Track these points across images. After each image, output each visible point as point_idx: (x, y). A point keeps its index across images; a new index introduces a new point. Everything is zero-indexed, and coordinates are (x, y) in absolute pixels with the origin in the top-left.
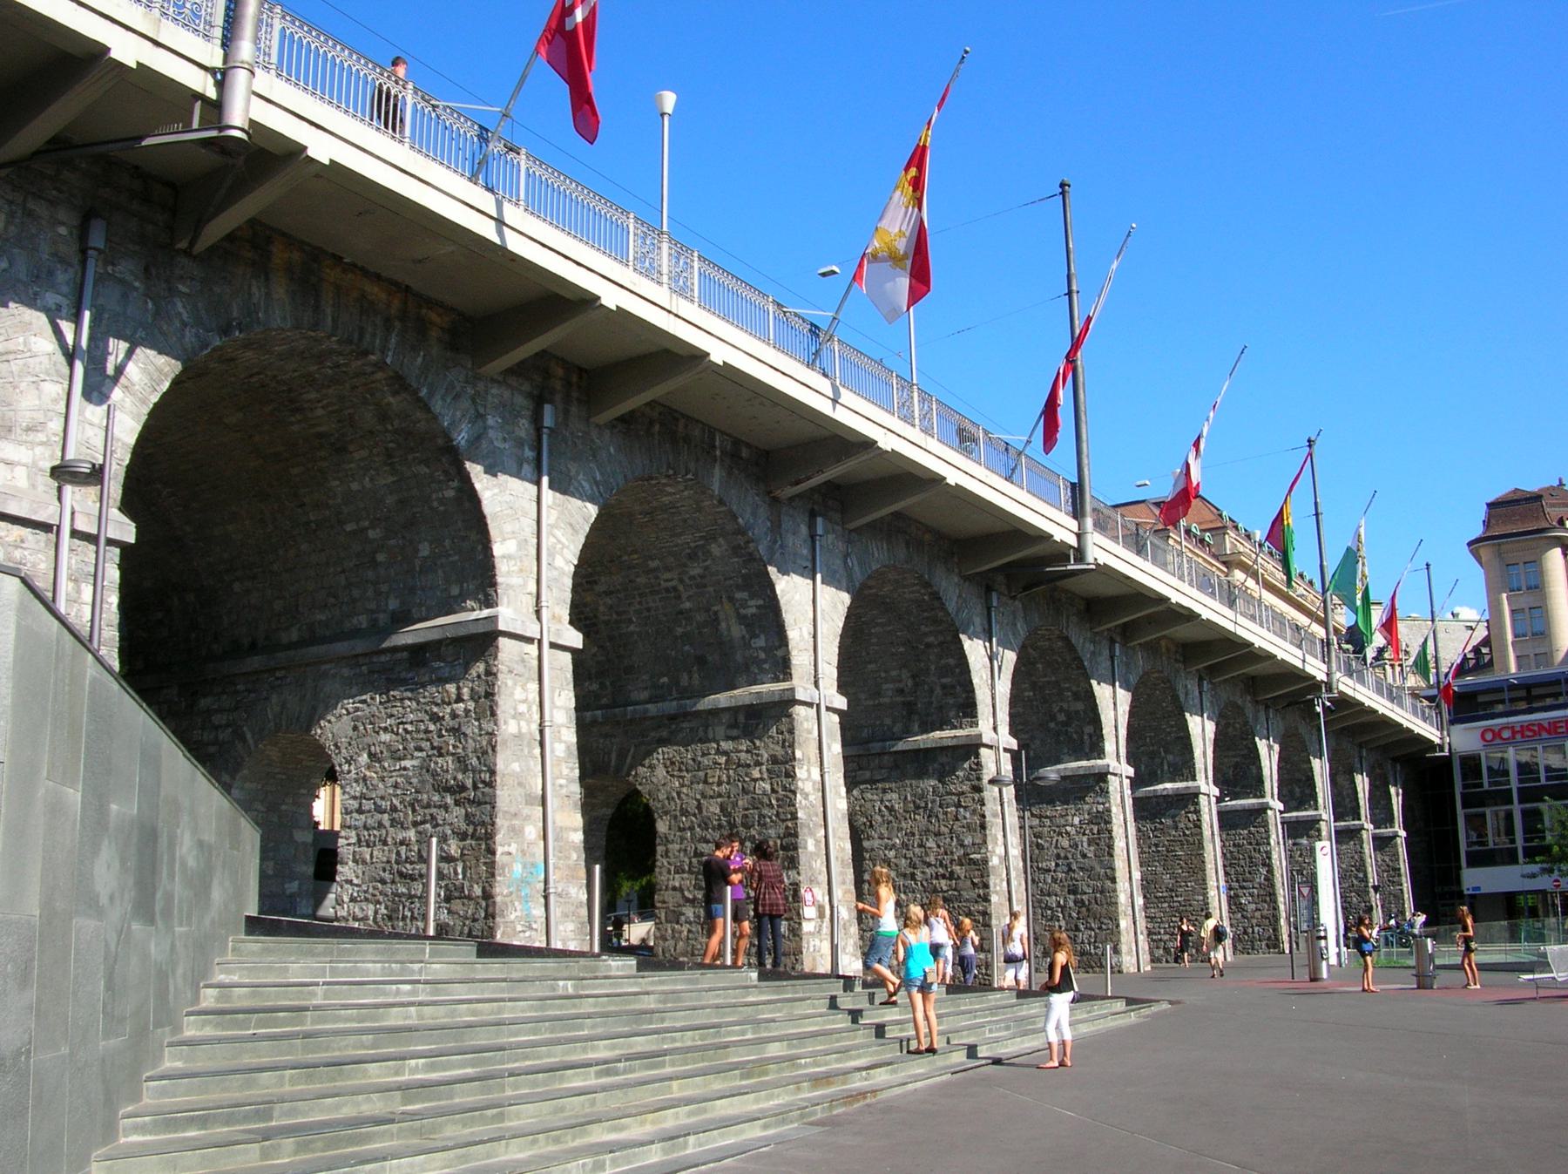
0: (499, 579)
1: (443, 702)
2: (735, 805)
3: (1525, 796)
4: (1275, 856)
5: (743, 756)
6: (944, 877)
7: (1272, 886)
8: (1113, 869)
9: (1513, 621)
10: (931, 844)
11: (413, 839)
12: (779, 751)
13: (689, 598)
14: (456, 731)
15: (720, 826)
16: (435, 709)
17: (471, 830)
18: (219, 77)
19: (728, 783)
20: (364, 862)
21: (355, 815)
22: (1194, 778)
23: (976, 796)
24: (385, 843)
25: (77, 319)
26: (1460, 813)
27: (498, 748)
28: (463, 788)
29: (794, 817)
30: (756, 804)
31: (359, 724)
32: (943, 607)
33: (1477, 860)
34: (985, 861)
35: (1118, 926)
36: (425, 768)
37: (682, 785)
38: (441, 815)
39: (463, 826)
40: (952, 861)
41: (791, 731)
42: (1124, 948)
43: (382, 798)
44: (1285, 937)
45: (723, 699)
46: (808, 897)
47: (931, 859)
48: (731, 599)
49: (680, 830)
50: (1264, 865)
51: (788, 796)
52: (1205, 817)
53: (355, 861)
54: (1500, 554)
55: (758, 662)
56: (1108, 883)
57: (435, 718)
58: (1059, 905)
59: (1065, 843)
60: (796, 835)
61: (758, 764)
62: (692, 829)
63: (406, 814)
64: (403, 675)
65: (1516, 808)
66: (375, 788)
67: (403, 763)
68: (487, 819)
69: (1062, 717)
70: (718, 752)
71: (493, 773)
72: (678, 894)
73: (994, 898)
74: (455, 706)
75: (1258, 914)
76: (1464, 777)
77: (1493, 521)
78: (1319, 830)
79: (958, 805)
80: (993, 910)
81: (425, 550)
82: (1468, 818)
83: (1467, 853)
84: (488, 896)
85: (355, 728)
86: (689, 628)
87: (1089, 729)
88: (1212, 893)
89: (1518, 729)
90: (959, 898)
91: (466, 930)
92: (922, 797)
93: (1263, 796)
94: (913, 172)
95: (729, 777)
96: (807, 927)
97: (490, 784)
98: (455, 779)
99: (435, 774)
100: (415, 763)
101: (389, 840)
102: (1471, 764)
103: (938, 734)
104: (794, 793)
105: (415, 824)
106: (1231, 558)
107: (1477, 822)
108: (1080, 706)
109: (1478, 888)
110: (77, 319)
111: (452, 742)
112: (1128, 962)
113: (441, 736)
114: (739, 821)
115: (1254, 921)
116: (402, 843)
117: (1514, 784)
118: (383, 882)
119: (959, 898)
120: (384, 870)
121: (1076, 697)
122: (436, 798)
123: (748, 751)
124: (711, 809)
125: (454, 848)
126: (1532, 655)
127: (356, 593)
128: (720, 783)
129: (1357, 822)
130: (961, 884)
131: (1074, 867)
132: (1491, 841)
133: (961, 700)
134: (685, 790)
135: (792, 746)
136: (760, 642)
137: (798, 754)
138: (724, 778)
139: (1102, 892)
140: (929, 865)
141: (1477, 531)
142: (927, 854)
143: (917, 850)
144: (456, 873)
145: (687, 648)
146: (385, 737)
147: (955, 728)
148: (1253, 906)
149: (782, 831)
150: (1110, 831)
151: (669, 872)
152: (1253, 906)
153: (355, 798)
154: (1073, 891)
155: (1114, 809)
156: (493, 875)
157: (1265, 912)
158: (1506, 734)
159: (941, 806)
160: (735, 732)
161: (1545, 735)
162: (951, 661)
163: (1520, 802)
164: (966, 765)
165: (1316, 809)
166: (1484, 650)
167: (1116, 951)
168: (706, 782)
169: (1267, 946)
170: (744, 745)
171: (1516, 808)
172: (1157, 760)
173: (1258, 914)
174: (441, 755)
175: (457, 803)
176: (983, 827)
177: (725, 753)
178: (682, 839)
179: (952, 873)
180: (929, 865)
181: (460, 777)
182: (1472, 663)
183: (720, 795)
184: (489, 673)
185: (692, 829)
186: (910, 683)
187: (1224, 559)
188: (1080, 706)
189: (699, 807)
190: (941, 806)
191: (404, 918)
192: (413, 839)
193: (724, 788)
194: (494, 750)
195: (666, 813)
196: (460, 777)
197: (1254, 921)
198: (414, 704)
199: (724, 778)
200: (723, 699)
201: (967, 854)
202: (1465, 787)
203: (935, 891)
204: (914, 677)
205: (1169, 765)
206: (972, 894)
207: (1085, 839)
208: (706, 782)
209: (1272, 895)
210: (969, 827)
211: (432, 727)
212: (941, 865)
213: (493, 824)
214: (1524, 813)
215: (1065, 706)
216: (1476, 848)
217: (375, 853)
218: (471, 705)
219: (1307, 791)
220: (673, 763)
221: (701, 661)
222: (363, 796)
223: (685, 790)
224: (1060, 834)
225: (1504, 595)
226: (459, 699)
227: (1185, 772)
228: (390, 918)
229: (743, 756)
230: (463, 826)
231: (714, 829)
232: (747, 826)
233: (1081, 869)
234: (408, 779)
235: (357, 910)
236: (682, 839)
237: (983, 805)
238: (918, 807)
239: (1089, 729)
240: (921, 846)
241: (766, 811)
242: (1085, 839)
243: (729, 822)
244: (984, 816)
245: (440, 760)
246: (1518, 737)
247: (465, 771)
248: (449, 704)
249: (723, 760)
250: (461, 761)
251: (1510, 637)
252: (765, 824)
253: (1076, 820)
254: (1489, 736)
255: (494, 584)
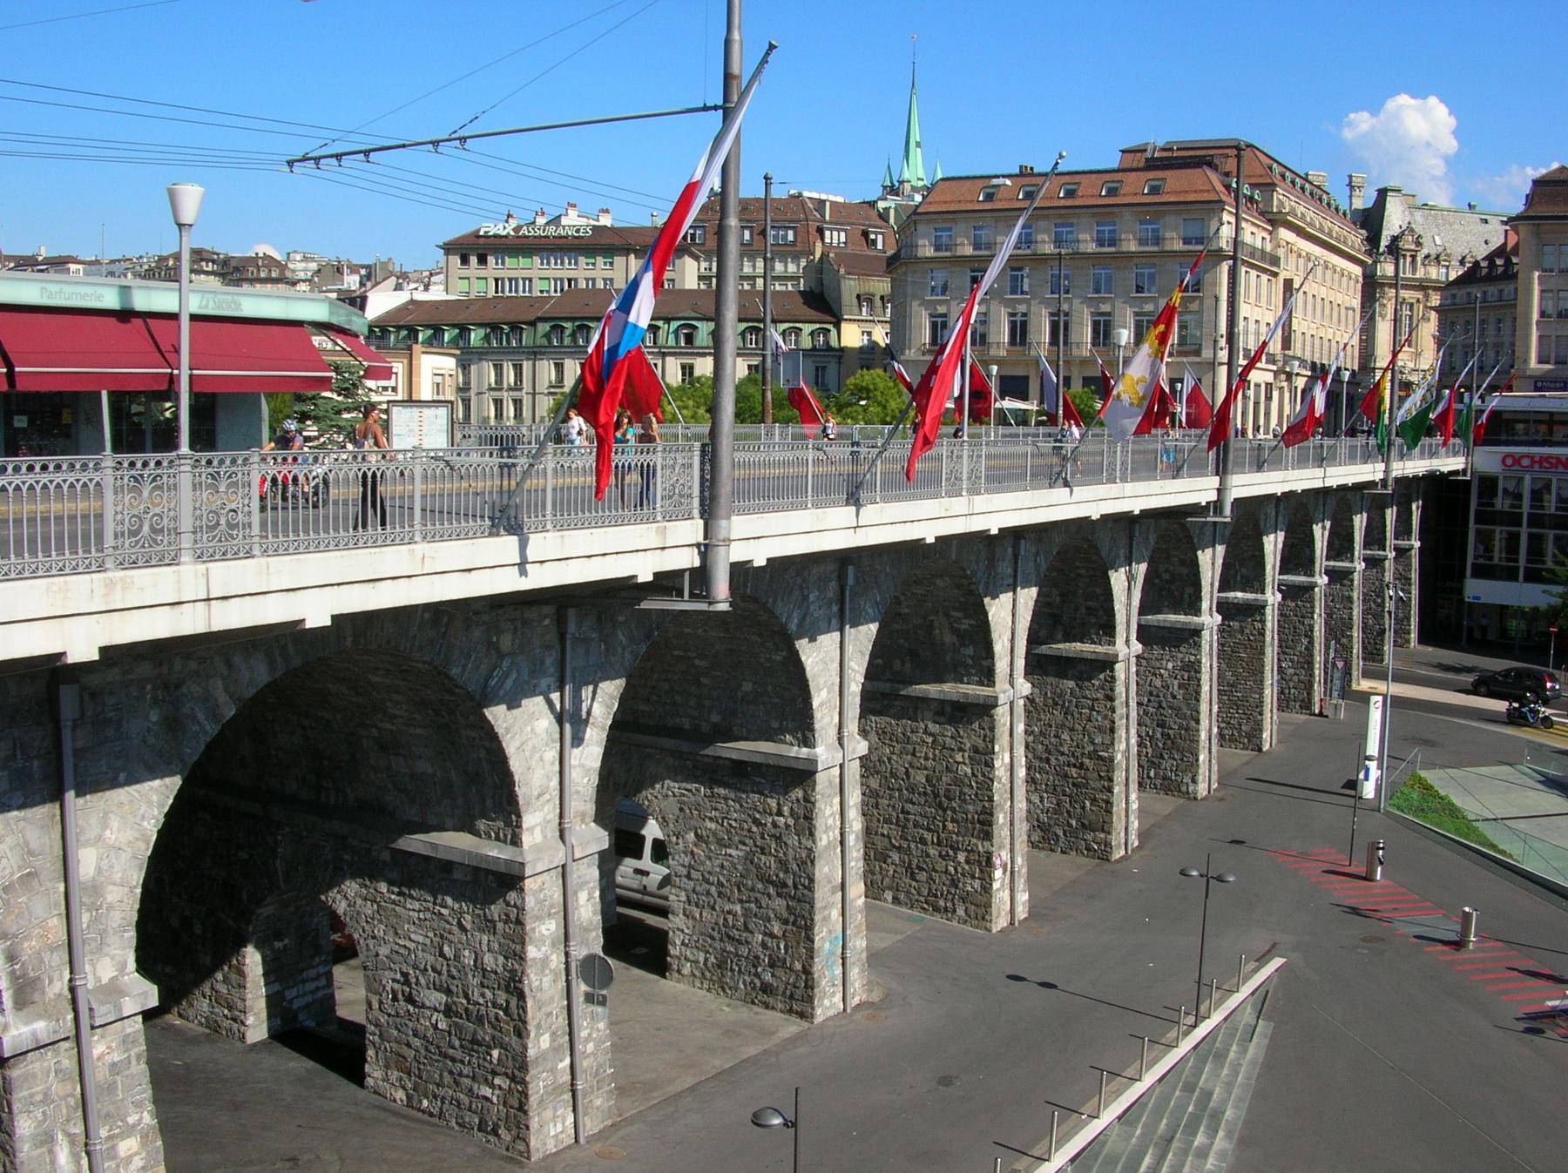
0: (817, 726)
1: (765, 812)
2: (939, 779)
3: (1535, 521)
4: (1316, 628)
5: (948, 740)
6: (1075, 766)
7: (1312, 656)
8: (1198, 713)
9: (1541, 299)
10: (1065, 736)
11: (739, 912)
12: (980, 743)
13: (908, 607)
14: (778, 838)
15: (925, 794)
16: (758, 816)
17: (792, 919)
18: (703, 549)
19: (934, 760)
20: (694, 918)
21: (684, 880)
22: (1263, 592)
23: (1109, 704)
24: (713, 908)
25: (561, 689)
26: (1472, 526)
27: (816, 862)
28: (784, 885)
29: (991, 800)
30: (958, 782)
31: (686, 808)
32: (1098, 554)
33: (1482, 572)
34: (1112, 760)
35: (1197, 760)
36: (749, 859)
37: (892, 753)
38: (764, 901)
39: (786, 915)
40: (1083, 754)
41: (992, 729)
42: (1200, 778)
43: (709, 873)
44: (1317, 699)
45: (932, 690)
46: (998, 862)
47: (1065, 749)
48: (947, 615)
49: (889, 788)
50: (1306, 636)
51: (987, 783)
52: (1269, 625)
53: (684, 914)
54: (1538, 234)
55: (967, 666)
56: (1193, 723)
57: (756, 822)
58: (1147, 734)
59: (1158, 683)
60: (991, 814)
61: (961, 750)
62: (900, 790)
63: (732, 891)
64: (726, 779)
65: (1524, 531)
66: (703, 864)
67: (729, 851)
68: (807, 915)
69: (1166, 576)
70: (925, 732)
71: (812, 880)
72: (886, 840)
73: (1116, 790)
74: (776, 818)
75: (1295, 678)
76: (1480, 496)
77: (1536, 199)
78: (1352, 581)
79: (1092, 709)
80: (1115, 800)
81: (747, 687)
82: (1478, 532)
83: (1473, 565)
84: (807, 972)
85: (681, 810)
86: (905, 627)
87: (1189, 590)
88: (1267, 692)
89: (1537, 459)
90: (1086, 786)
91: (788, 993)
92: (1061, 696)
93: (1313, 576)
94: (1162, 327)
95: (934, 755)
96: (996, 885)
97: (810, 888)
98: (777, 876)
99: (758, 867)
100: (741, 854)
101: (717, 908)
102: (1488, 484)
103: (1078, 646)
104: (992, 781)
105: (741, 901)
106: (1277, 217)
107: (1485, 539)
108: (1184, 571)
109: (1478, 598)
110: (561, 689)
111: (773, 846)
112: (1202, 789)
113: (763, 838)
114: (942, 793)
115: (1291, 684)
116: (729, 912)
117: (1526, 509)
118: (713, 938)
119: (1086, 786)
120: (713, 929)
121: (1182, 563)
122: (760, 886)
123: (952, 737)
124: (918, 778)
125: (776, 928)
126: (1553, 338)
127: (678, 699)
128: (926, 759)
129: (1381, 553)
130: (1089, 775)
131: (1164, 705)
132: (1498, 556)
133: (1102, 622)
134: (894, 757)
135: (992, 741)
136: (970, 651)
137: (997, 748)
138: (931, 755)
139: (1186, 730)
140: (1063, 754)
141: (1518, 207)
142: (1061, 745)
143: (1053, 740)
144: (779, 948)
145: (902, 641)
146: (713, 826)
147: (1093, 642)
148: (1292, 671)
149: (979, 809)
150: (1199, 680)
151: (879, 821)
152: (1292, 671)
153: (683, 866)
154: (1162, 725)
155: (1204, 660)
156: (812, 958)
157: (1302, 677)
158: (1525, 462)
159: (1076, 706)
160: (942, 719)
161: (1561, 469)
162: (1098, 591)
163: (1529, 526)
164: (1102, 676)
165: (1352, 561)
166: (1499, 262)
167: (1194, 781)
168: (914, 754)
169: (1300, 706)
170: (950, 730)
171: (1524, 531)
172: (1233, 572)
173: (1295, 678)
174: (763, 853)
175: (779, 895)
176: (1112, 730)
177: (931, 734)
178: (891, 797)
179: (1082, 764)
180: (1063, 754)
181: (781, 875)
182: (1484, 271)
183: (926, 769)
184: (807, 800)
185: (900, 790)
186: (1058, 599)
187: (1271, 217)
188: (1184, 571)
189: (907, 773)
190: (1076, 706)
191: (732, 970)
192: (739, 912)
193: (930, 763)
194: (812, 862)
195: (877, 773)
196: (781, 875)
197: (1291, 684)
198: (738, 806)
199: (931, 755)
200: (932, 690)
201: (1096, 751)
202: (1479, 505)
203: (1066, 776)
204: (1061, 595)
205: (1242, 577)
206: (1098, 785)
207: (1176, 682)
208: (914, 754)
209: (1310, 663)
210: (1099, 729)
211: (754, 829)
212: (1073, 755)
213: (812, 920)
214: (1530, 536)
215: (1171, 568)
216: (1481, 561)
217: (704, 914)
218: (791, 822)
219: (1346, 545)
220: (884, 732)
221: (913, 653)
222: (690, 867)
223: (894, 757)
224: (1154, 674)
225: (1537, 274)
226: (780, 813)
227: (1256, 584)
228: (719, 967)
229: (948, 740)
230: (786, 915)
231: (919, 794)
232: (950, 799)
233: (1170, 707)
234: (734, 865)
235: (688, 953)
236: (891, 797)
237: (1114, 712)
238: (1057, 704)
239: (1189, 590)
240: (1056, 736)
241: (966, 790)
242: (1176, 682)
243: (933, 792)
244: (1114, 722)
245: (763, 858)
246: (1536, 468)
247: (786, 871)
248: (771, 814)
249: (930, 740)
250: (783, 865)
251: (1535, 316)
252: (965, 800)
253: (1170, 665)
254: (1509, 461)
255: (812, 730)
